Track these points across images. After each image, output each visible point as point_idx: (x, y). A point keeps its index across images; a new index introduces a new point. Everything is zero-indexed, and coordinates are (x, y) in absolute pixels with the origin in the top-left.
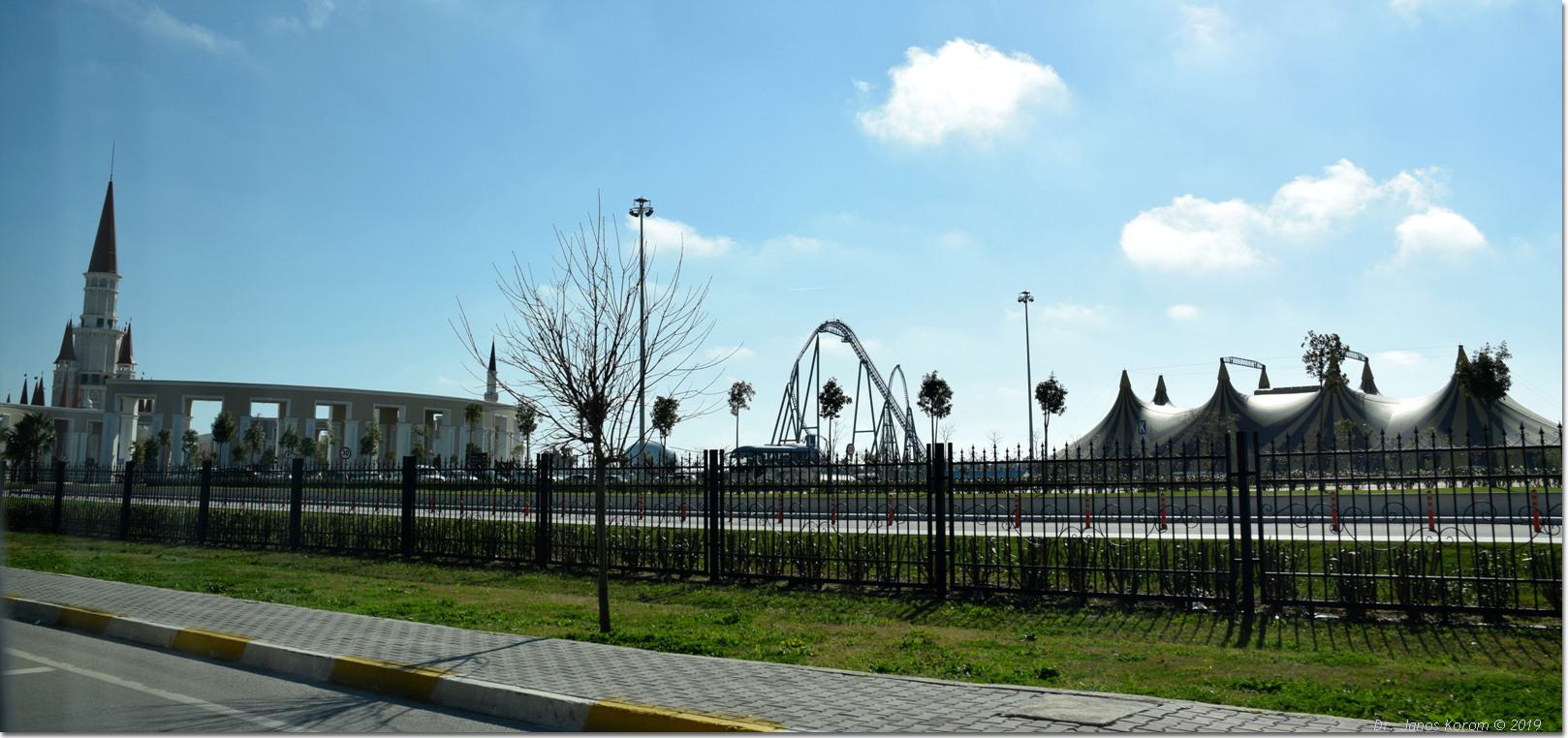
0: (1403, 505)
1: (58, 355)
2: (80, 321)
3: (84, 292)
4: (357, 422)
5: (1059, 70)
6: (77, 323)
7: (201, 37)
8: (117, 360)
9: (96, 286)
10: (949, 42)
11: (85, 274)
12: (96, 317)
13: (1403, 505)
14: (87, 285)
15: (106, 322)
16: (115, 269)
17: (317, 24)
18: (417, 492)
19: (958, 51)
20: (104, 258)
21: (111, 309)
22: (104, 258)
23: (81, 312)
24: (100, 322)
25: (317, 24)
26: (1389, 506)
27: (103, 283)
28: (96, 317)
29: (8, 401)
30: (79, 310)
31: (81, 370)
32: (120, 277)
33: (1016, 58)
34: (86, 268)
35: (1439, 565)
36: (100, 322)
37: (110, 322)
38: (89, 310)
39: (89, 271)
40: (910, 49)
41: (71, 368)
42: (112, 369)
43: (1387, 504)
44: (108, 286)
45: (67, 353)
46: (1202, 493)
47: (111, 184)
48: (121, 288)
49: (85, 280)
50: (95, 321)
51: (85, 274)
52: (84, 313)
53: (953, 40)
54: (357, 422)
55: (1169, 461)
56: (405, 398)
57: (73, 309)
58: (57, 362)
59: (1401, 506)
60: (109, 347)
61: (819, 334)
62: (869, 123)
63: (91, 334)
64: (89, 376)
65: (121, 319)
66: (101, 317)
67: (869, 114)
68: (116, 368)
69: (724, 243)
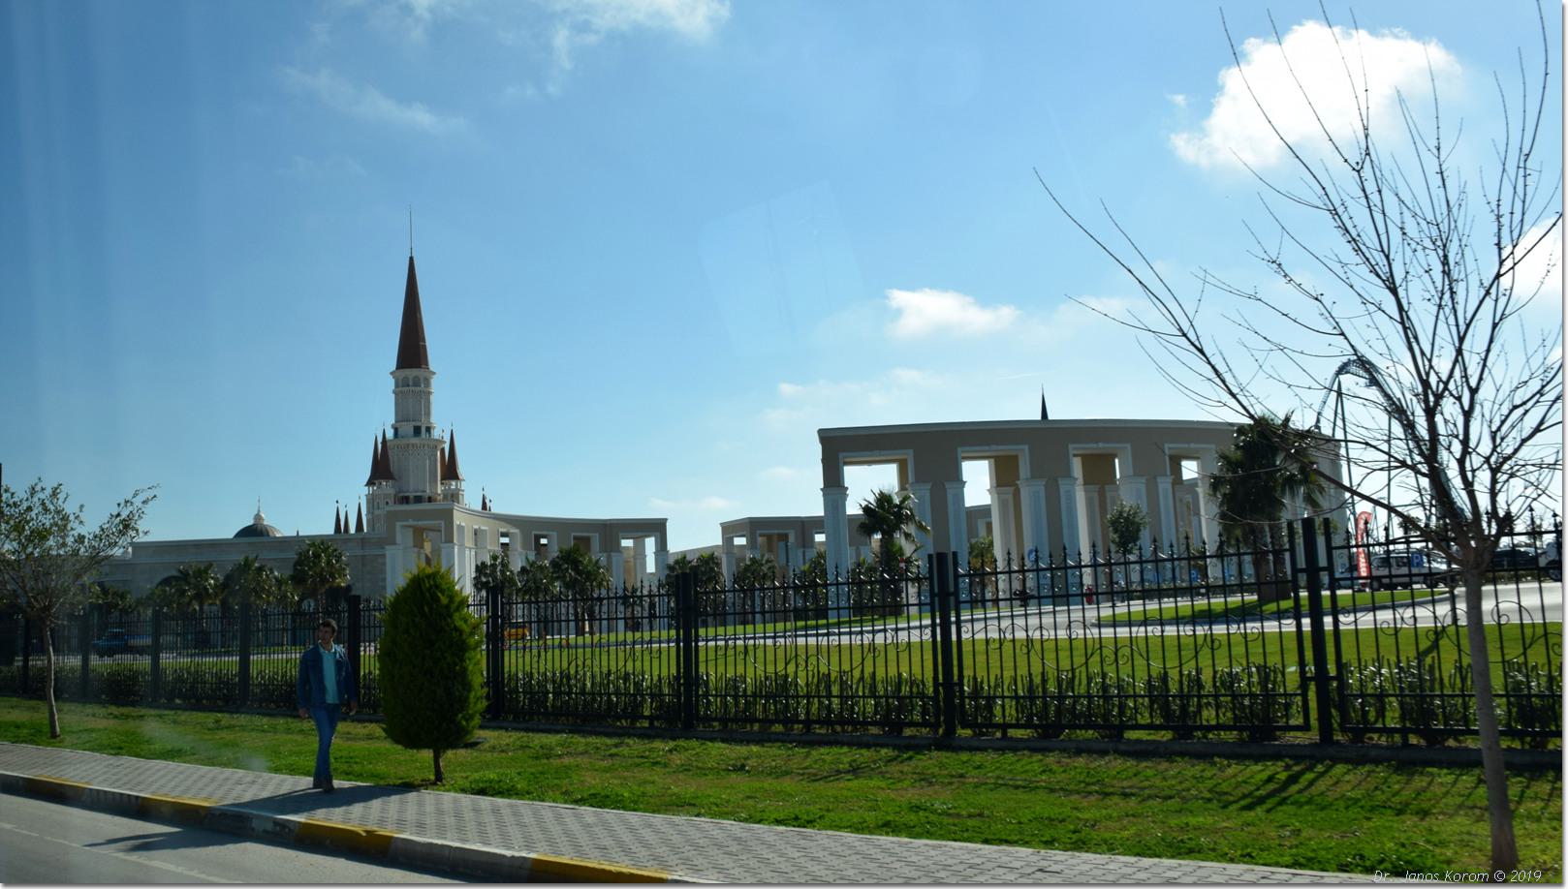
0: (1519, 604)
1: (369, 474)
2: (392, 431)
3: (393, 396)
4: (1143, 480)
5: (1448, 44)
6: (390, 434)
7: (422, 117)
8: (439, 478)
9: (408, 385)
10: (1296, 27)
11: (391, 373)
12: (412, 424)
13: (1519, 604)
14: (397, 386)
15: (423, 430)
16: (427, 364)
17: (552, 90)
18: (251, 657)
19: (1310, 37)
20: (412, 352)
21: (428, 414)
22: (412, 352)
23: (392, 420)
24: (417, 431)
25: (552, 90)
26: (1521, 651)
27: (417, 383)
28: (412, 424)
29: (484, 506)
30: (390, 419)
31: (400, 492)
32: (434, 373)
33: (1383, 36)
34: (393, 366)
35: (719, 676)
36: (417, 431)
37: (428, 429)
38: (402, 416)
39: (398, 368)
40: (1247, 41)
41: (386, 487)
42: (436, 489)
43: (1498, 603)
44: (422, 386)
45: (381, 468)
46: (1096, 614)
47: (411, 259)
48: (434, 382)
49: (393, 381)
50: (412, 430)
51: (391, 373)
52: (396, 422)
53: (1300, 24)
54: (1143, 480)
55: (1007, 575)
56: (629, 524)
57: (380, 417)
58: (370, 483)
59: (1517, 606)
60: (430, 459)
61: (1340, 376)
62: (1184, 146)
63: (408, 445)
64: (411, 497)
65: (440, 430)
66: (418, 424)
67: (1185, 136)
68: (440, 489)
69: (1006, 313)
